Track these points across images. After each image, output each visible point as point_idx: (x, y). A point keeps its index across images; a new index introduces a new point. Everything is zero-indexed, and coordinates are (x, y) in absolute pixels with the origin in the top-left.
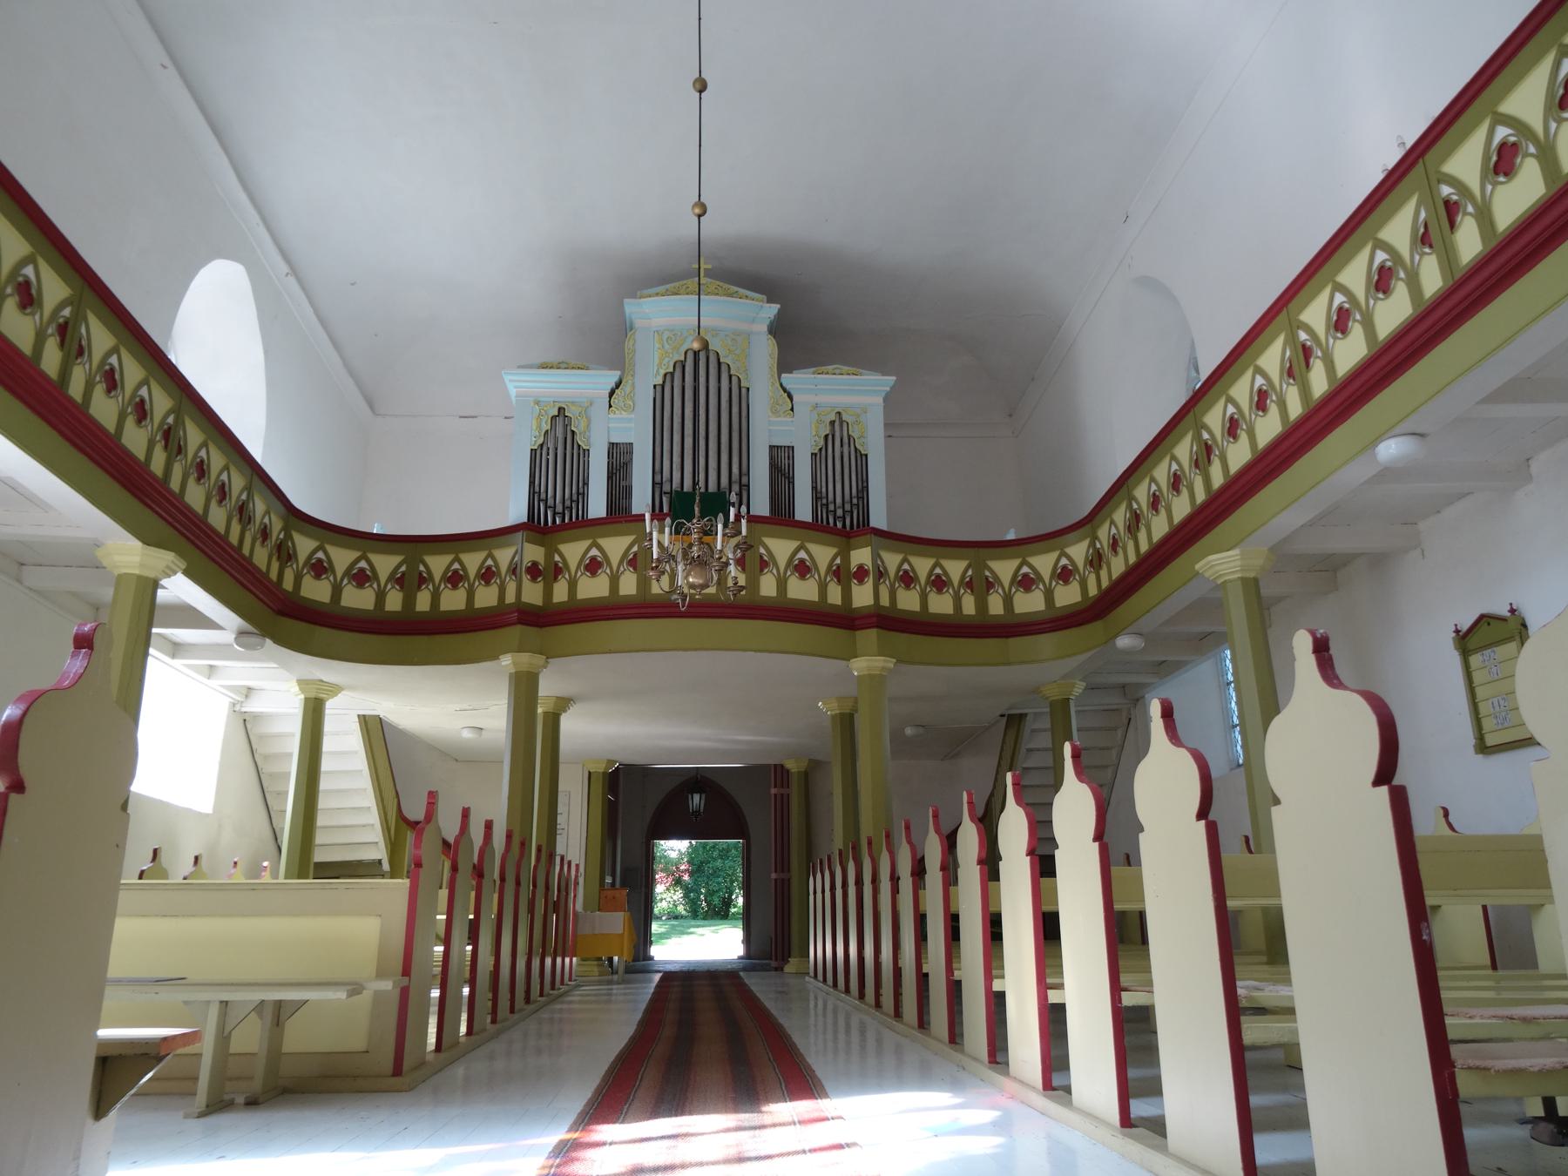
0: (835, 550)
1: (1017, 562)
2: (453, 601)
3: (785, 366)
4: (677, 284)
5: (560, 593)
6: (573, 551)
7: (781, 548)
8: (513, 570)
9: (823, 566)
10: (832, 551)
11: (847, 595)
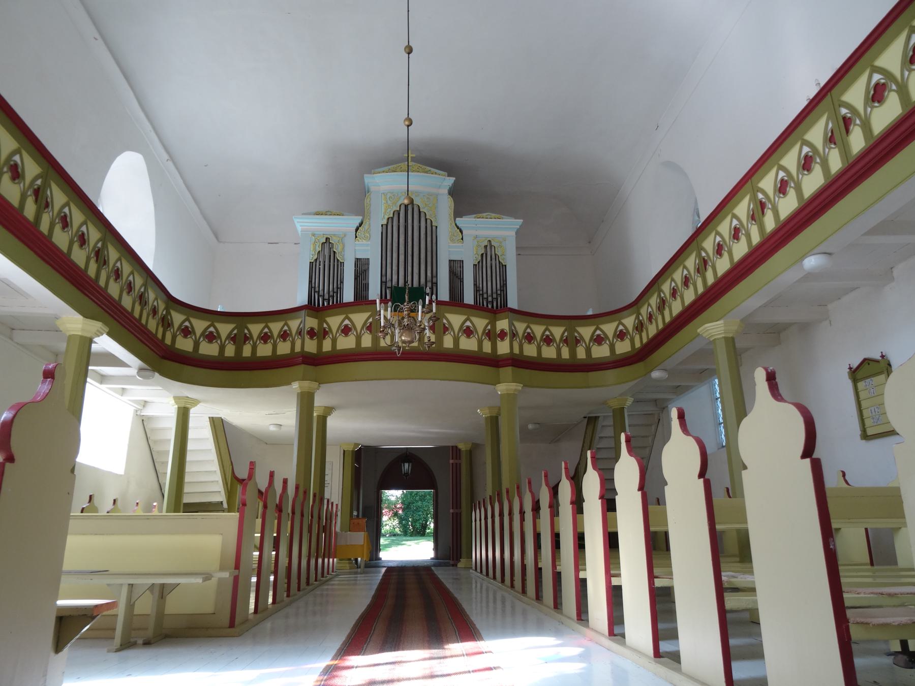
0: (487, 321)
1: (593, 328)
2: (264, 350)
3: (458, 213)
4: (395, 166)
5: (327, 346)
6: (334, 322)
7: (456, 320)
8: (300, 333)
9: (480, 330)
10: (486, 321)
11: (494, 347)
